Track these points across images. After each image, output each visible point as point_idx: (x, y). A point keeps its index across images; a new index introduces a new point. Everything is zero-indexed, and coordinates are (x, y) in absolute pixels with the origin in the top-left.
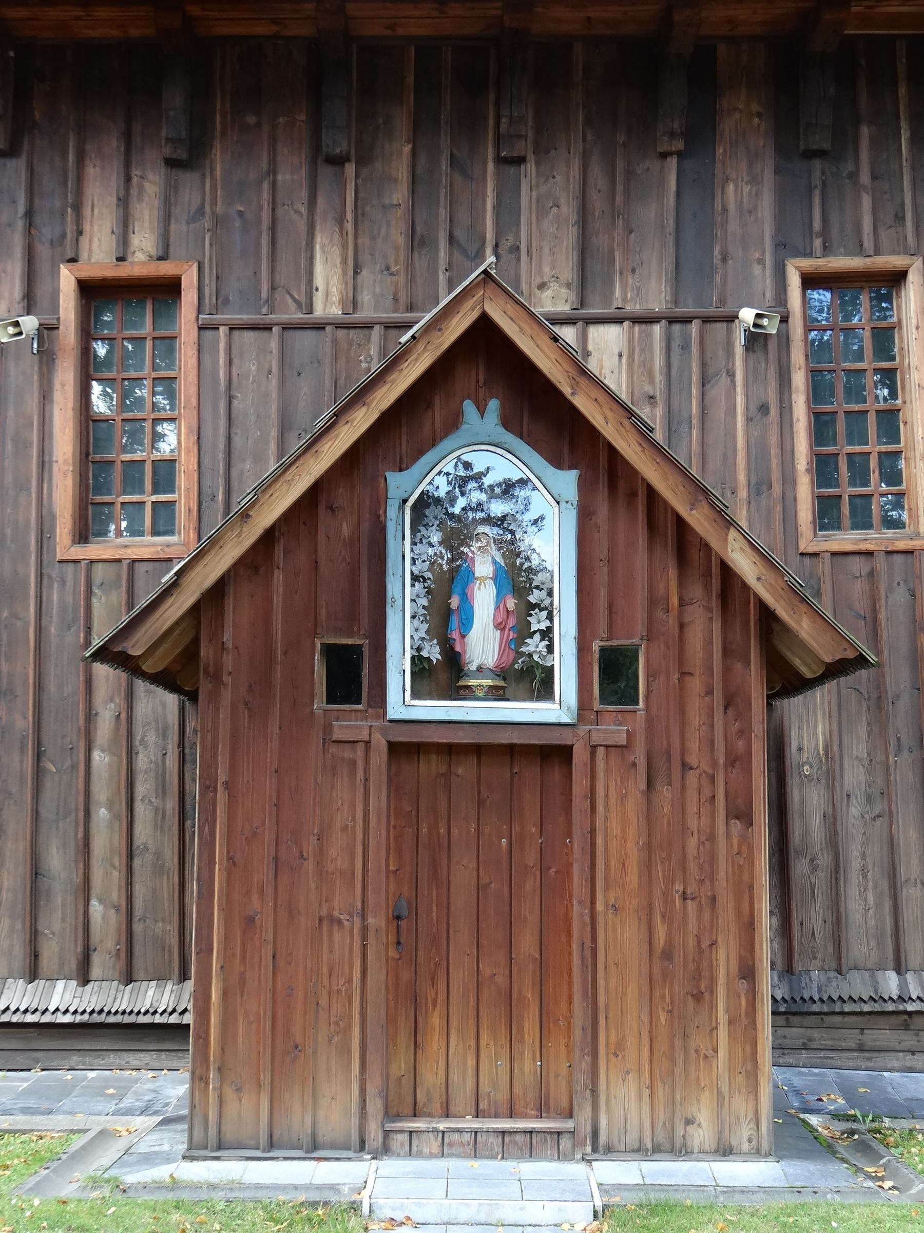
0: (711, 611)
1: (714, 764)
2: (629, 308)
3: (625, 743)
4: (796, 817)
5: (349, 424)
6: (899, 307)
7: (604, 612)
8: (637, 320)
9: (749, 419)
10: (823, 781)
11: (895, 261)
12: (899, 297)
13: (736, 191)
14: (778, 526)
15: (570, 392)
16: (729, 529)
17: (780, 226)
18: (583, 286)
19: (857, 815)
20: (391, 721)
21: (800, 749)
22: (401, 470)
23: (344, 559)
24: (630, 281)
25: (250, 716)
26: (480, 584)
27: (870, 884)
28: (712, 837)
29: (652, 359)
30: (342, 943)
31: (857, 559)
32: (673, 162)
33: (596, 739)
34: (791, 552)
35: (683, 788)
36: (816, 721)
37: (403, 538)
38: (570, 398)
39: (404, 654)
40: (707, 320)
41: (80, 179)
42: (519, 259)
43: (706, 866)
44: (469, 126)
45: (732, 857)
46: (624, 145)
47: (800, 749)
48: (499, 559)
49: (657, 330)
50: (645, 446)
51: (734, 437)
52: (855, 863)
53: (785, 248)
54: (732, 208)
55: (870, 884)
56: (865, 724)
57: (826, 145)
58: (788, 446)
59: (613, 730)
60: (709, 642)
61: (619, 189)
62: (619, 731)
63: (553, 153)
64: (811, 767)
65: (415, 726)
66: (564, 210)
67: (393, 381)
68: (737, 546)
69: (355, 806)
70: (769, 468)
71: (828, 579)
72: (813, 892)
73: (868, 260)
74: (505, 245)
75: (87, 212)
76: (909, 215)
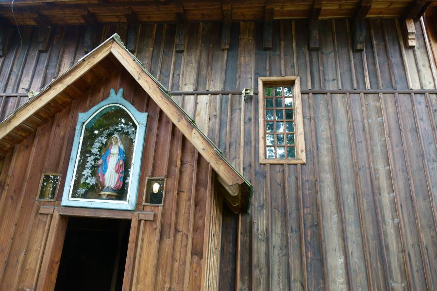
0: (193, 166)
1: (188, 230)
2: (210, 90)
4: (255, 254)
6: (293, 92)
8: (213, 94)
9: (245, 122)
10: (265, 241)
11: (292, 78)
12: (293, 89)
13: (244, 59)
14: (253, 155)
15: (137, 78)
16: (193, 129)
17: (257, 68)
18: (197, 84)
19: (277, 255)
20: (63, 206)
21: (258, 229)
23: (59, 144)
24: (211, 83)
25: (12, 202)
27: (281, 280)
28: (184, 263)
29: (216, 105)
30: (338, 254)
31: (279, 166)
32: (226, 52)
33: (141, 217)
34: (257, 163)
35: (175, 240)
36: (263, 220)
37: (81, 136)
38: (137, 80)
40: (233, 94)
41: (62, 58)
42: (179, 78)
43: (181, 276)
44: (170, 43)
45: (193, 273)
46: (212, 47)
47: (258, 229)
48: (122, 147)
49: (218, 97)
51: (240, 127)
52: (276, 272)
53: (257, 75)
54: (243, 64)
55: (281, 280)
56: (280, 221)
57: (270, 46)
58: (257, 131)
59: (148, 213)
60: (191, 179)
61: (210, 58)
62: (150, 214)
63: (192, 50)
64: (261, 236)
66: (194, 64)
67: (74, 75)
68: (195, 136)
70: (251, 138)
71: (268, 172)
72: (260, 282)
73: (283, 77)
74: (176, 73)
75: (62, 66)
76: (295, 65)
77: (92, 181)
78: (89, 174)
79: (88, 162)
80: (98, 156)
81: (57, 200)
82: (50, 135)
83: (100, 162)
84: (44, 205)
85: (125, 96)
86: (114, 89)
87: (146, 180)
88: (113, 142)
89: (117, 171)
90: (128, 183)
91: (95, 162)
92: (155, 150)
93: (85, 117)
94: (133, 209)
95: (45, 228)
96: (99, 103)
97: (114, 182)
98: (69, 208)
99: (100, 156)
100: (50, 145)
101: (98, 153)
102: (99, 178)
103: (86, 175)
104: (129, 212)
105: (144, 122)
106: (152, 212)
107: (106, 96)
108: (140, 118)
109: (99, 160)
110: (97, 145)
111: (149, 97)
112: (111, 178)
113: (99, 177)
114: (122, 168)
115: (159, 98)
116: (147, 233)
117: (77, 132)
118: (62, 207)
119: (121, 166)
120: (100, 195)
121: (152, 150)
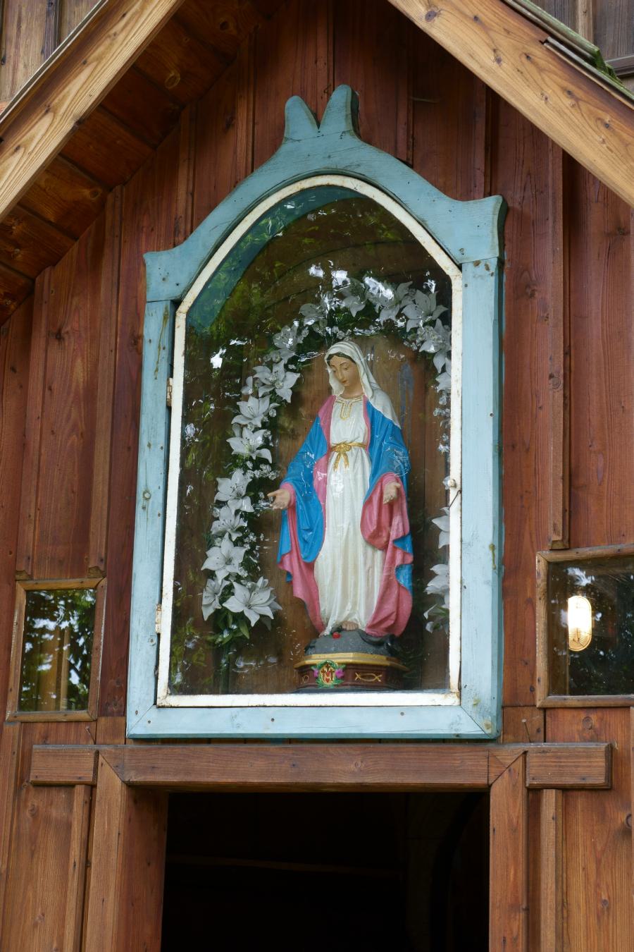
3: (600, 780)
5: (22, 150)
7: (555, 486)
22: (175, 246)
26: (337, 459)
33: (539, 772)
37: (171, 375)
38: (422, 24)
39: (160, 602)
48: (382, 404)
50: (579, 93)
62: (588, 755)
65: (178, 749)
67: (99, 59)
69: (64, 920)
77: (252, 603)
78: (236, 568)
79: (221, 504)
80: (266, 468)
81: (103, 712)
82: (23, 387)
83: (283, 496)
84: (45, 739)
85: (363, 128)
86: (303, 95)
87: (540, 567)
88: (333, 383)
89: (374, 538)
90: (441, 597)
91: (255, 501)
92: (567, 398)
93: (182, 273)
94: (489, 732)
95: (67, 854)
96: (235, 184)
97: (369, 594)
98: (167, 748)
99: (273, 466)
100: (34, 438)
101: (266, 454)
102: (290, 583)
103: (221, 575)
104: (466, 747)
105: (488, 250)
106: (595, 738)
107: (270, 141)
108: (459, 231)
109: (274, 485)
110: (254, 409)
111: (494, 100)
112: (348, 579)
113: (289, 575)
114: (397, 520)
115: (553, 100)
116: (582, 858)
117: (150, 354)
118: (131, 745)
119: (391, 505)
120: (305, 670)
121: (550, 401)
